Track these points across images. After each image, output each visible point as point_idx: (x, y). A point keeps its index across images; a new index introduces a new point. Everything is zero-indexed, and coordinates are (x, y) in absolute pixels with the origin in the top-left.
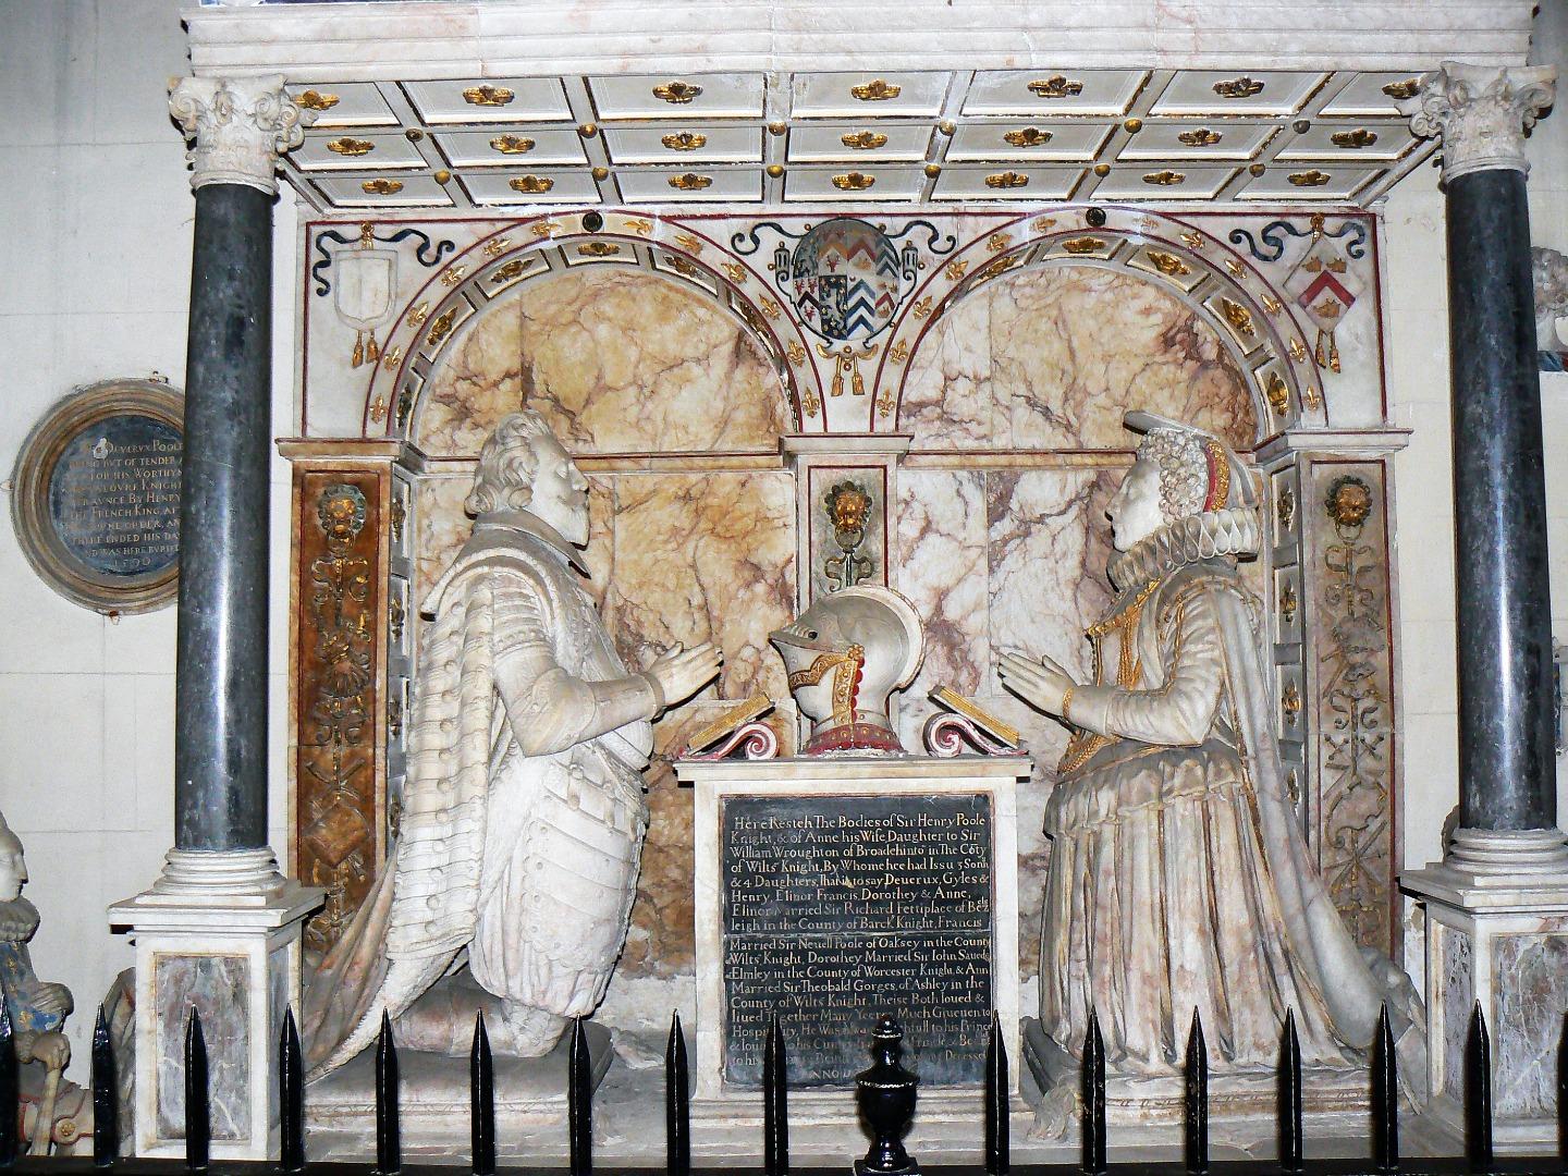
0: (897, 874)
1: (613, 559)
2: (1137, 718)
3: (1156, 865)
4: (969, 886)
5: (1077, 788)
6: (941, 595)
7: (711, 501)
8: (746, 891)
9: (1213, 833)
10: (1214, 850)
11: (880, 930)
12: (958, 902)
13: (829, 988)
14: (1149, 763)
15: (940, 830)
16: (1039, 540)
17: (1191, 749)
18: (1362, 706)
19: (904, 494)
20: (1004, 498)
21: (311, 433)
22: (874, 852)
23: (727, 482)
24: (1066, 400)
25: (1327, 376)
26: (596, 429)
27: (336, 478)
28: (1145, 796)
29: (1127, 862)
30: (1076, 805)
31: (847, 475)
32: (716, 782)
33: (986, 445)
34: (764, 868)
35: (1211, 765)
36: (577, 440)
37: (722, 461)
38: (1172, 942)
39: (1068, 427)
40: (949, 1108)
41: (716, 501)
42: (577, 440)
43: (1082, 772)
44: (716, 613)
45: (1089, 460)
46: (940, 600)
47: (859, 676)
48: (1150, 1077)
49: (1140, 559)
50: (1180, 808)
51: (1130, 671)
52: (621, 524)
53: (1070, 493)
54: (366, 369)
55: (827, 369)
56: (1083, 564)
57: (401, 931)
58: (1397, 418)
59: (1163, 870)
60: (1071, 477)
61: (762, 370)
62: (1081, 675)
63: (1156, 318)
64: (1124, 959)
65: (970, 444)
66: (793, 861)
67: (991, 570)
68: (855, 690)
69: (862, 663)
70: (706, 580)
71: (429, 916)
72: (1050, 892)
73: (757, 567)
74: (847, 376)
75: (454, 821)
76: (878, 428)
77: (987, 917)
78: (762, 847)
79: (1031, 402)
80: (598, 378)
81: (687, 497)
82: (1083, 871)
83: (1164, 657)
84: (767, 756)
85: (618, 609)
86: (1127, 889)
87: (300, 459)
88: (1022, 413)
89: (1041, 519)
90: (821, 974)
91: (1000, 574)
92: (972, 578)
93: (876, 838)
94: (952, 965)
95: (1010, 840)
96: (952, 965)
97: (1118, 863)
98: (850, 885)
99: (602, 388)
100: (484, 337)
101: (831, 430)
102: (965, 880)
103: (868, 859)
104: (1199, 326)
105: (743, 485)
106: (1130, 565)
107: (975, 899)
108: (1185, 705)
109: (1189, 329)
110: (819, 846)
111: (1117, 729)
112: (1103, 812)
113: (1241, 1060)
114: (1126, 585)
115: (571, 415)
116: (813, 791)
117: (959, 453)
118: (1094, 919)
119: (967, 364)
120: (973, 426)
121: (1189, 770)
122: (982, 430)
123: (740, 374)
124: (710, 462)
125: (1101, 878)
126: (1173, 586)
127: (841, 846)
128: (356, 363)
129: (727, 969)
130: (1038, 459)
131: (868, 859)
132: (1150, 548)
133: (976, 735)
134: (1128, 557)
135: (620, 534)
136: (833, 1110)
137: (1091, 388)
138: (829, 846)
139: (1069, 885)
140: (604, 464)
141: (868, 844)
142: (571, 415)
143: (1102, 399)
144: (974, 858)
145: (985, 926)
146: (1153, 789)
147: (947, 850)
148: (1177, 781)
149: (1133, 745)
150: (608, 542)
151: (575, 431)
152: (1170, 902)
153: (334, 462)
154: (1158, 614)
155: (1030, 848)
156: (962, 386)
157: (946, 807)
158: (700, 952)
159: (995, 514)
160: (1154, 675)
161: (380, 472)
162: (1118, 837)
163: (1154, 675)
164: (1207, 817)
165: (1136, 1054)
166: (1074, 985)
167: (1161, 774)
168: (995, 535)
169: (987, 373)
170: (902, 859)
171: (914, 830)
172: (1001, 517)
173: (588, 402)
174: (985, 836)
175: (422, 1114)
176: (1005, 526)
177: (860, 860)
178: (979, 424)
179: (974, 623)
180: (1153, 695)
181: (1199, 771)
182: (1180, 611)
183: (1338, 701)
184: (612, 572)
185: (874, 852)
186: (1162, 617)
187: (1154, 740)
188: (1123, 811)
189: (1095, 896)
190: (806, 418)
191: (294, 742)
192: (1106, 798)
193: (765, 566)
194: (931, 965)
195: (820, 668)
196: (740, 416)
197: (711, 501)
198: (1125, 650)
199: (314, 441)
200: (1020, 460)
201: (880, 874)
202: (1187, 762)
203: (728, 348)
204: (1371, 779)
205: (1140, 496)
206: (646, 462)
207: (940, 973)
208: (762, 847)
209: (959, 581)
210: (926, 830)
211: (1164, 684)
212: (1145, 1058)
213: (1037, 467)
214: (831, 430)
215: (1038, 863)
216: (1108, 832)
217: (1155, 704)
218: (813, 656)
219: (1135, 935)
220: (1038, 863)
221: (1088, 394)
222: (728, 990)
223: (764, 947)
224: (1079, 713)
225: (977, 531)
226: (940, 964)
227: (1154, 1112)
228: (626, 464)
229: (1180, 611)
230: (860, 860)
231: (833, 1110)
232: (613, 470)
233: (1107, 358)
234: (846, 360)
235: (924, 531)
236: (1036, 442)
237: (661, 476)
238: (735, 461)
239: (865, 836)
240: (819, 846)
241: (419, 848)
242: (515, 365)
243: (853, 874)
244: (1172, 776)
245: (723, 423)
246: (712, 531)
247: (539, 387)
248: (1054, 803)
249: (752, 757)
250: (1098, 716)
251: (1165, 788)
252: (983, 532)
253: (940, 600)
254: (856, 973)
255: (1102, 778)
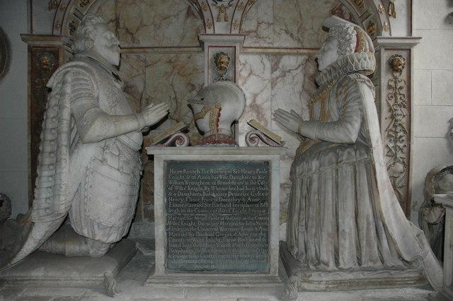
0: (233, 192)
1: (145, 82)
2: (329, 133)
3: (335, 190)
4: (261, 197)
5: (303, 160)
6: (255, 96)
7: (178, 63)
8: (174, 197)
9: (357, 178)
10: (358, 184)
11: (226, 213)
12: (256, 203)
13: (206, 235)
14: (333, 150)
15: (249, 175)
16: (289, 78)
17: (351, 145)
18: (399, 135)
19: (243, 62)
20: (277, 64)
21: (34, 33)
22: (224, 183)
23: (184, 57)
24: (298, 32)
25: (391, 19)
26: (140, 38)
27: (44, 50)
28: (330, 163)
29: (323, 189)
30: (303, 167)
31: (222, 50)
32: (162, 155)
33: (271, 46)
34: (181, 189)
35: (358, 151)
36: (134, 42)
37: (182, 49)
38: (340, 221)
39: (299, 40)
40: (251, 281)
41: (180, 63)
42: (134, 42)
43: (305, 153)
44: (179, 101)
45: (306, 51)
46: (255, 98)
47: (219, 115)
48: (330, 272)
49: (330, 72)
50: (344, 168)
51: (323, 114)
52: (148, 70)
53: (299, 63)
54: (53, 11)
55: (215, 12)
56: (303, 86)
57: (36, 211)
58: (415, 34)
59: (337, 192)
60: (299, 57)
61: (196, 20)
62: (306, 117)
63: (329, 5)
64: (320, 225)
65: (266, 45)
66: (192, 186)
67: (272, 88)
68: (218, 120)
69: (220, 110)
70: (176, 90)
71: (47, 206)
72: (292, 198)
73: (193, 85)
74: (222, 15)
75: (55, 168)
76: (233, 33)
77: (268, 209)
78: (181, 180)
79: (287, 32)
80: (141, 22)
81: (170, 62)
82: (305, 192)
83: (339, 109)
84: (183, 146)
85: (147, 99)
86: (322, 199)
87: (30, 42)
88: (284, 35)
89: (289, 71)
90: (203, 230)
91: (276, 89)
92: (266, 91)
93: (225, 178)
94: (253, 227)
95: (280, 173)
96: (253, 227)
97: (319, 189)
98: (214, 196)
99: (142, 25)
100: (103, 8)
101: (216, 32)
102: (259, 194)
103: (222, 186)
104: (343, 8)
105: (189, 58)
106: (325, 75)
107: (263, 202)
108: (349, 126)
109: (340, 9)
110: (202, 181)
111: (320, 137)
112: (314, 169)
113: (363, 266)
114: (323, 83)
115: (132, 34)
116: (200, 159)
117: (262, 48)
118: (309, 210)
119: (265, 19)
120: (267, 40)
121: (349, 153)
122: (271, 41)
123: (189, 21)
124: (177, 50)
125: (312, 194)
126: (343, 81)
127: (211, 181)
128: (50, 8)
129: (167, 227)
130: (289, 51)
131: (222, 186)
132: (333, 67)
133: (264, 138)
134: (325, 71)
135: (148, 74)
136: (207, 281)
137: (307, 27)
138: (206, 181)
139: (299, 196)
140: (142, 50)
141: (222, 180)
142: (132, 34)
143: (310, 32)
144: (263, 186)
145: (267, 212)
146: (334, 160)
147: (252, 183)
148: (344, 157)
149: (325, 143)
150: (143, 77)
151: (133, 39)
152: (340, 205)
153: (43, 44)
154: (337, 92)
155: (283, 181)
156: (263, 26)
157: (252, 165)
158: (156, 221)
159: (274, 69)
160: (335, 116)
161: (59, 47)
162: (319, 178)
163: (335, 116)
164: (355, 172)
165: (324, 263)
166: (300, 234)
167: (338, 155)
168: (274, 76)
169: (272, 22)
170: (233, 186)
171: (240, 174)
172: (276, 70)
173: (137, 30)
174: (267, 178)
175: (49, 280)
176: (277, 73)
177: (219, 186)
178: (269, 39)
179: (266, 105)
180: (335, 123)
181: (353, 153)
182: (346, 91)
183: (391, 133)
184: (145, 87)
185: (224, 183)
186: (339, 92)
187: (335, 141)
188: (322, 169)
189: (309, 202)
190: (207, 30)
191: (30, 141)
192: (315, 164)
193: (196, 85)
194: (245, 227)
195: (205, 110)
196: (188, 35)
197: (178, 63)
198: (323, 107)
199: (34, 35)
200: (282, 51)
201: (227, 192)
202: (349, 150)
203: (184, 12)
204: (401, 160)
205: (329, 49)
206: (156, 49)
207: (249, 230)
208: (181, 180)
209: (262, 91)
210: (245, 175)
211: (339, 119)
212: (327, 265)
213: (289, 54)
214: (216, 32)
215: (286, 186)
216: (315, 177)
217: (336, 127)
218: (201, 107)
219: (326, 217)
220: (286, 186)
221: (306, 30)
222: (168, 235)
223: (181, 219)
224: (305, 131)
225: (267, 75)
226: (249, 226)
227: (330, 286)
228: (149, 50)
229: (346, 91)
230: (219, 186)
231: (207, 281)
232: (145, 52)
233: (313, 18)
234: (221, 9)
235: (250, 74)
236: (287, 45)
237: (161, 55)
238: (186, 49)
239: (221, 177)
240: (202, 181)
241: (44, 179)
242: (114, 18)
243: (216, 192)
244: (342, 155)
245: (183, 37)
246: (178, 73)
247: (121, 25)
248: (294, 166)
249: (178, 145)
250: (313, 133)
251: (339, 160)
252: (269, 75)
253: (255, 98)
254: (216, 229)
255: (313, 156)
